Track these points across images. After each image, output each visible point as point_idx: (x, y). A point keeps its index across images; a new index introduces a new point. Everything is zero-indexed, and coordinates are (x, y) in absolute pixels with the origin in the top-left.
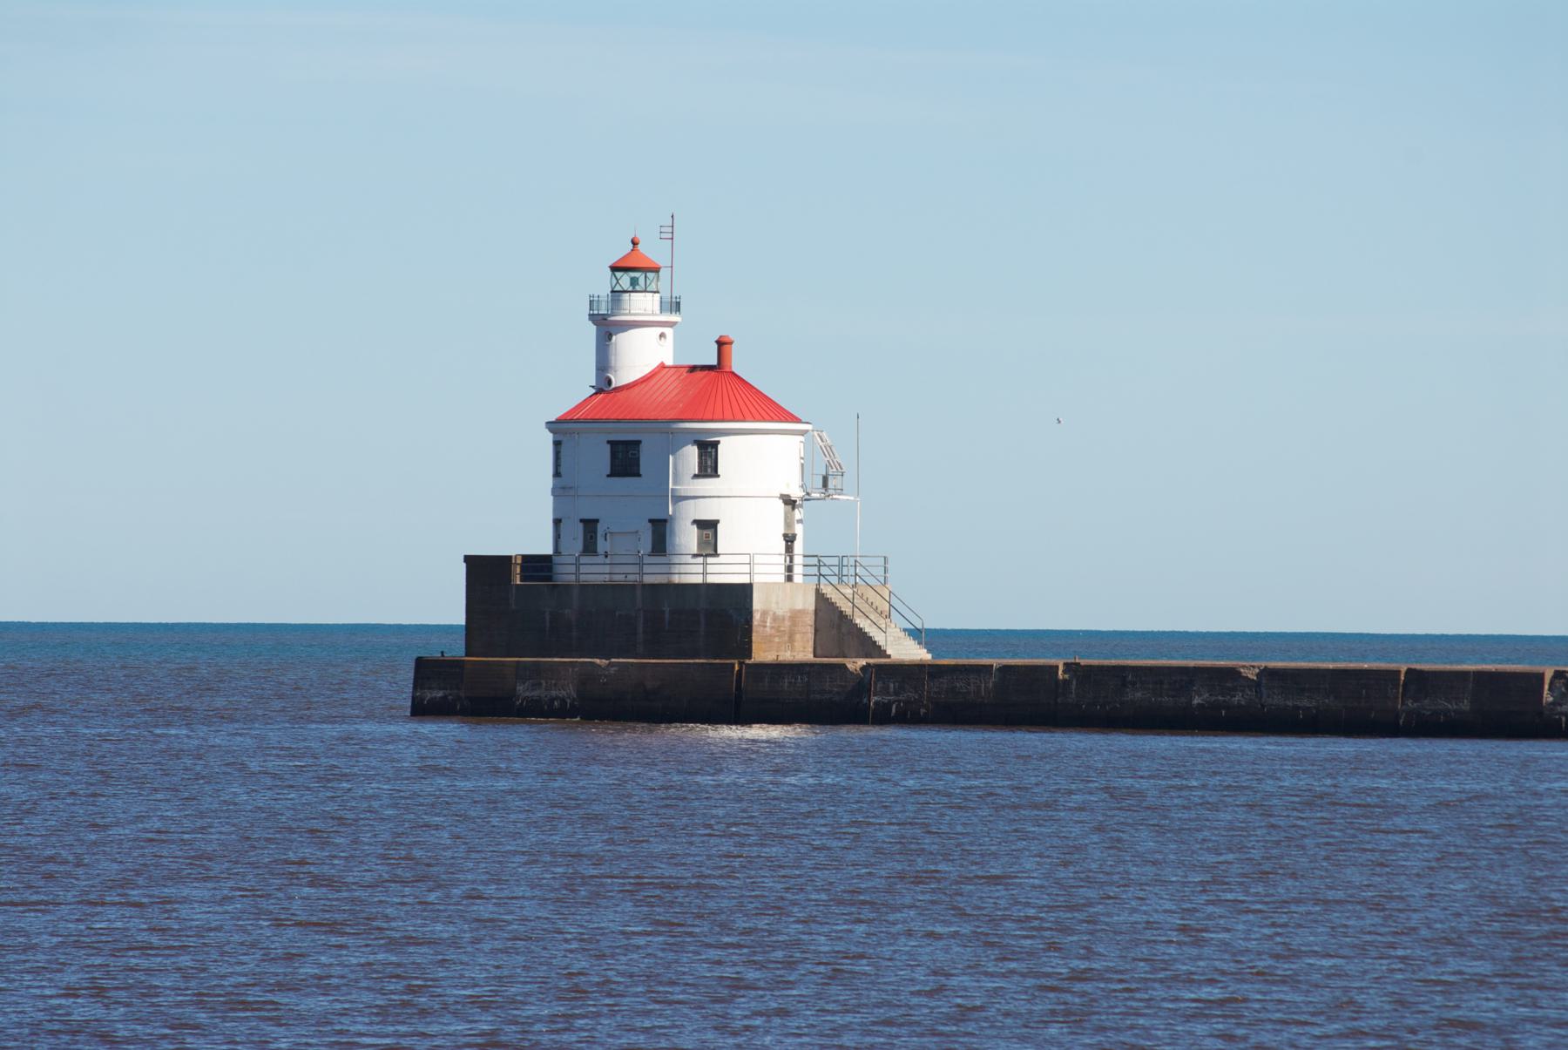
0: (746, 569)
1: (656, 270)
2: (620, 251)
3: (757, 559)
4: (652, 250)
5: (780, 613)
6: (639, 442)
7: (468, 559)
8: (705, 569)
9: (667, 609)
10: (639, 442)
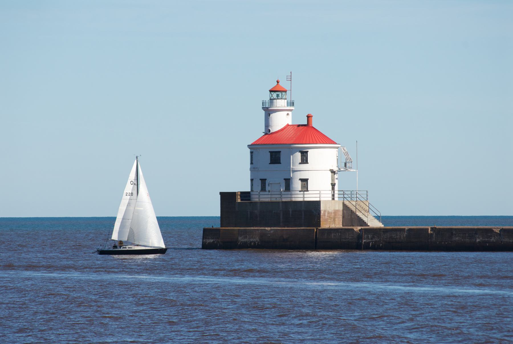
0: (318, 196)
1: (285, 91)
2: (273, 85)
3: (322, 192)
4: (284, 84)
5: (330, 211)
6: (280, 152)
7: (222, 194)
8: (304, 196)
9: (291, 210)
10: (280, 152)
